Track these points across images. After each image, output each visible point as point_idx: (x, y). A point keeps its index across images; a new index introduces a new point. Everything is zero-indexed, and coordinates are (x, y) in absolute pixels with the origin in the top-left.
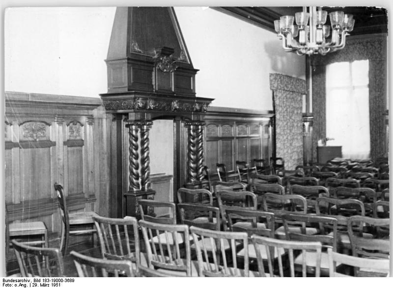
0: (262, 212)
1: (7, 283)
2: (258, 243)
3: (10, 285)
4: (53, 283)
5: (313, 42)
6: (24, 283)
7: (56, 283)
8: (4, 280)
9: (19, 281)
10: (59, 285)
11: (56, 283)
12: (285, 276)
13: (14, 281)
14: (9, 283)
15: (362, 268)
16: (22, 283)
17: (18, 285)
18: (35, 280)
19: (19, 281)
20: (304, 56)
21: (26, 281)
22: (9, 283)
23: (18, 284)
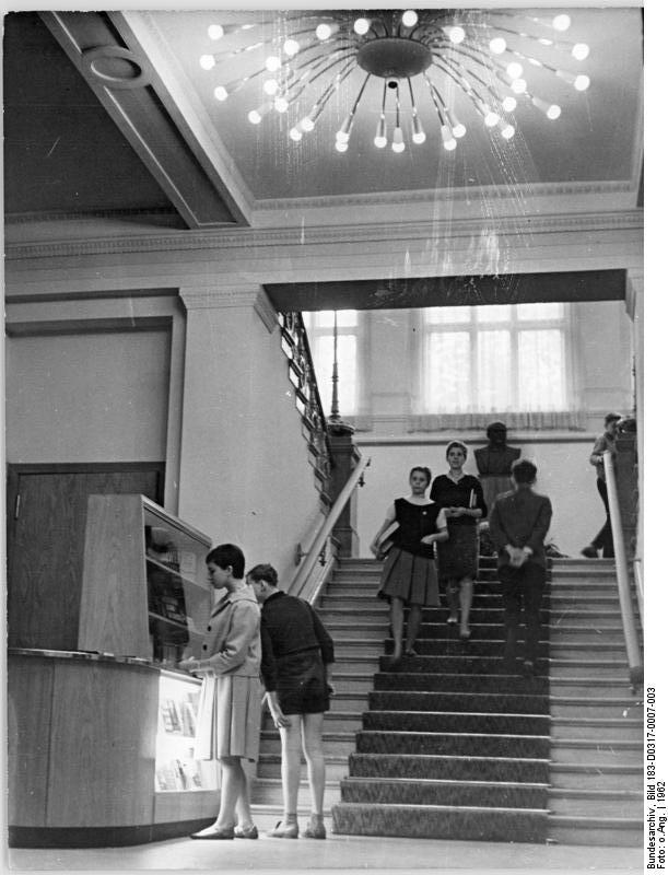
0: (174, 572)
1: (657, 860)
2: (367, 793)
3: (662, 852)
4: (657, 798)
5: (314, 68)
6: (657, 822)
7: (657, 792)
8: (651, 867)
9: (652, 832)
10: (651, 742)
11: (657, 792)
12: (262, 734)
13: (652, 844)
14: (657, 854)
15: (514, 429)
16: (657, 826)
17: (661, 835)
18: (651, 798)
19: (652, 832)
20: (190, 226)
21: (653, 816)
22: (657, 854)
23: (658, 835)
